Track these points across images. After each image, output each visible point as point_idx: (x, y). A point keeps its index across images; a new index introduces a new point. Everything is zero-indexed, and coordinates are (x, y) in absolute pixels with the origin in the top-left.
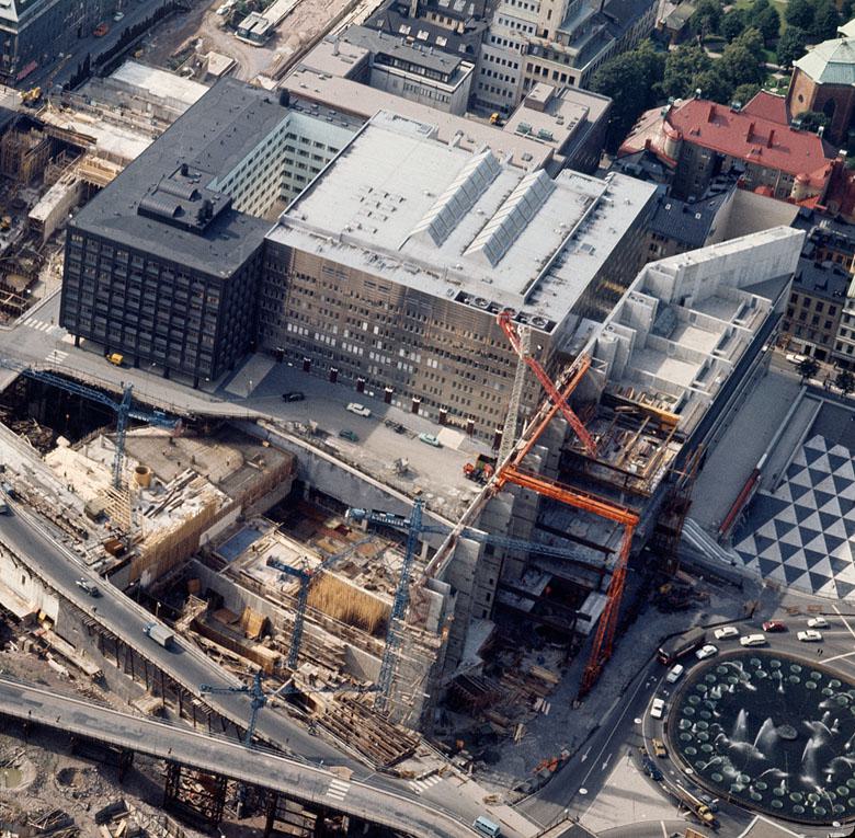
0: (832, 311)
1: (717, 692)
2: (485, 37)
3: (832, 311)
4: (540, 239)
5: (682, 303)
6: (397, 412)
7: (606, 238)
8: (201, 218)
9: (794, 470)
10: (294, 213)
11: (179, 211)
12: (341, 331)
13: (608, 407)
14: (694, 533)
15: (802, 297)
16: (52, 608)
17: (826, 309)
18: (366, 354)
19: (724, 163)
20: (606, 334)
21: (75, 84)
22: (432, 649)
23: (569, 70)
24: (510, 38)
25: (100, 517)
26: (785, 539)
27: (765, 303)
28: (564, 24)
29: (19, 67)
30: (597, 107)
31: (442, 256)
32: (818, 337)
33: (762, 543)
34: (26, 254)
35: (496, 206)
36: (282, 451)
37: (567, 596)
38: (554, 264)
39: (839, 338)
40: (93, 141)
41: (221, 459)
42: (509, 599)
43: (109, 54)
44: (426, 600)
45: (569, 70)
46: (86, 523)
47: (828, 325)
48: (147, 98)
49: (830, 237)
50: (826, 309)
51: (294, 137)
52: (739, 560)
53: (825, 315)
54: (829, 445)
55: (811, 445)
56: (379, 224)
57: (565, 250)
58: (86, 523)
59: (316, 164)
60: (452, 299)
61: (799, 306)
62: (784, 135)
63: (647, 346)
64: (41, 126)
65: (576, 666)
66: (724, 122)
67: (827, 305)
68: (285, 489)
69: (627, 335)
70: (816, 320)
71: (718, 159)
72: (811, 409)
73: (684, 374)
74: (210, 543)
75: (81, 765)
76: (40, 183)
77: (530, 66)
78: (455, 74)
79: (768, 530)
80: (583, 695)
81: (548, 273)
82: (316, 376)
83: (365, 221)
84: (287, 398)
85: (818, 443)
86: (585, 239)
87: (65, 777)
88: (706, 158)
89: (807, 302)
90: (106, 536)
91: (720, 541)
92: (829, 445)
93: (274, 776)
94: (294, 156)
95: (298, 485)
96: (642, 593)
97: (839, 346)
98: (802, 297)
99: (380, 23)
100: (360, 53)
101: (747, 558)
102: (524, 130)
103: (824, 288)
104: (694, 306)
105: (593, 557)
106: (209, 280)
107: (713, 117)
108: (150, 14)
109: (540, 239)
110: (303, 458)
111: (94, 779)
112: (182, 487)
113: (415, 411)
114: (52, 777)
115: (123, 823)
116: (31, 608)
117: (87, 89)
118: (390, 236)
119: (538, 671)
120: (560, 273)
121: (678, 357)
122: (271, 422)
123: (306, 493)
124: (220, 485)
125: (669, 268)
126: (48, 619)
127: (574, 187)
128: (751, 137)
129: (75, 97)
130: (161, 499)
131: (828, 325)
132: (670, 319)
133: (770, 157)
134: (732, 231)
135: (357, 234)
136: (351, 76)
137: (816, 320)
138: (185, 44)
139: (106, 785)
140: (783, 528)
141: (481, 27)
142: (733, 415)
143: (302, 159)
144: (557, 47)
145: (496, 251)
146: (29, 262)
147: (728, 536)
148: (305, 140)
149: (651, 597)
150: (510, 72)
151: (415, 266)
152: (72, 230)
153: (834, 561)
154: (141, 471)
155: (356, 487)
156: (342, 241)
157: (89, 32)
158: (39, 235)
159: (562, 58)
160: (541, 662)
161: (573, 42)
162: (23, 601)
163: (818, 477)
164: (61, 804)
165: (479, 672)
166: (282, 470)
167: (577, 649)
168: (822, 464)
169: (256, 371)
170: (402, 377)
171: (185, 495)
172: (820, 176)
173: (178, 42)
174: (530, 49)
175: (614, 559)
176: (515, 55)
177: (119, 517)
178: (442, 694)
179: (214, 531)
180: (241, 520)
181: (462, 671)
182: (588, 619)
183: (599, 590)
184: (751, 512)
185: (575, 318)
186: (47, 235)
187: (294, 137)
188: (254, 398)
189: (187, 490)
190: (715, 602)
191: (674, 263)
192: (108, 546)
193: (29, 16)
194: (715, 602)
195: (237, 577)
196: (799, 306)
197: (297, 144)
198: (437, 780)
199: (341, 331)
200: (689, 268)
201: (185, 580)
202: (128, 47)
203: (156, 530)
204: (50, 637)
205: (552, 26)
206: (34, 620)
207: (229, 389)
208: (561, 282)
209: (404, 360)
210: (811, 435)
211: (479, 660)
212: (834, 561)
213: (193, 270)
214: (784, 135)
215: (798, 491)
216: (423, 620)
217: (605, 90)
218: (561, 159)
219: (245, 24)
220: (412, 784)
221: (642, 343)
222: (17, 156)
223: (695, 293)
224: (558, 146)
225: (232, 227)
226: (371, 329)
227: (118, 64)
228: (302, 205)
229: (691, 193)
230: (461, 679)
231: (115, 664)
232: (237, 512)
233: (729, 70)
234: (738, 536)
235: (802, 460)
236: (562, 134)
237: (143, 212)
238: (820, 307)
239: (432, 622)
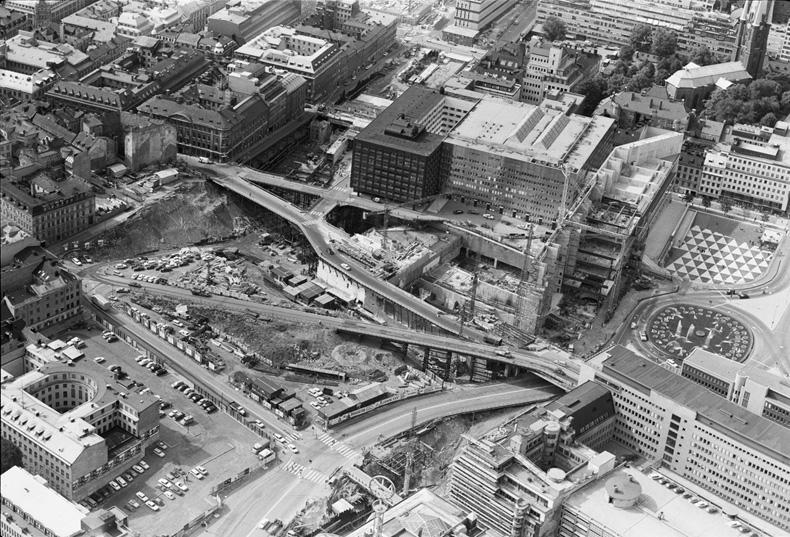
0: (697, 173)
1: (666, 319)
2: (524, 74)
3: (697, 173)
4: (566, 139)
5: (632, 164)
6: (506, 217)
8: (413, 133)
9: (687, 239)
10: (453, 132)
11: (403, 131)
12: (478, 182)
13: (606, 202)
14: (647, 260)
15: (683, 167)
16: (361, 296)
17: (695, 171)
18: (490, 191)
20: (602, 172)
21: (339, 103)
22: (541, 292)
23: (564, 87)
24: (535, 74)
25: (379, 258)
27: (669, 164)
28: (560, 67)
29: (315, 95)
30: (580, 99)
31: (524, 146)
32: (692, 186)
34: (326, 169)
36: (456, 235)
37: (594, 283)
38: (573, 148)
39: (702, 185)
40: (351, 123)
41: (428, 239)
42: (570, 282)
43: (353, 91)
44: (537, 270)
45: (564, 87)
46: (374, 260)
47: (696, 179)
48: (373, 107)
49: (692, 144)
50: (695, 171)
53: (694, 175)
54: (702, 230)
55: (694, 229)
57: (577, 143)
58: (374, 260)
59: (451, 124)
61: (682, 172)
62: (666, 104)
63: (619, 181)
64: (327, 119)
65: (601, 311)
66: (638, 100)
67: (695, 170)
68: (457, 252)
69: (611, 173)
70: (690, 177)
71: (638, 115)
72: (692, 215)
73: (639, 189)
74: (427, 272)
75: (386, 353)
76: (328, 142)
78: (513, 89)
79: (679, 261)
80: (607, 322)
81: (571, 151)
82: (473, 204)
83: (486, 134)
84: (456, 213)
85: (697, 228)
87: (379, 357)
88: (632, 117)
89: (686, 170)
90: (383, 265)
91: (659, 264)
92: (702, 230)
93: (473, 350)
94: (447, 123)
95: (463, 250)
96: (627, 283)
97: (702, 188)
98: (683, 167)
100: (469, 81)
103: (693, 162)
105: (607, 263)
106: (419, 157)
107: (633, 98)
108: (369, 76)
109: (566, 139)
110: (466, 237)
111: (391, 358)
112: (412, 249)
113: (514, 216)
114: (373, 357)
115: (408, 373)
116: (352, 298)
117: (345, 104)
118: (498, 139)
119: (585, 313)
121: (633, 185)
122: (449, 222)
123: (467, 254)
124: (430, 248)
125: (625, 149)
126: (360, 302)
127: (577, 122)
128: (651, 106)
129: (340, 107)
130: (404, 253)
131: (696, 179)
132: (627, 170)
133: (660, 114)
134: (648, 135)
136: (466, 88)
137: (690, 177)
138: (385, 89)
139: (397, 361)
140: (686, 261)
141: (521, 71)
142: (659, 214)
143: (451, 118)
144: (558, 77)
145: (548, 142)
146: (328, 172)
147: (663, 262)
148: (453, 109)
149: (632, 284)
150: (537, 89)
151: (511, 150)
153: (711, 273)
154: (394, 242)
155: (491, 247)
156: (476, 142)
157: (343, 82)
158: (331, 161)
160: (586, 310)
161: (564, 75)
162: (348, 295)
164: (379, 367)
165: (558, 313)
166: (457, 242)
167: (601, 305)
168: (700, 236)
169: (440, 203)
170: (507, 200)
171: (413, 252)
172: (685, 120)
173: (381, 88)
174: (545, 78)
175: (615, 263)
176: (537, 82)
177: (389, 258)
178: (543, 322)
179: (428, 266)
180: (440, 263)
181: (551, 312)
182: (607, 287)
183: (609, 279)
184: (670, 255)
185: (585, 172)
186: (335, 161)
188: (442, 212)
189: (415, 250)
190: (660, 286)
191: (627, 146)
192: (384, 268)
193: (319, 72)
194: (660, 286)
195: (443, 285)
196: (682, 172)
197: (449, 111)
198: (547, 351)
199: (478, 182)
201: (417, 282)
202: (361, 87)
203: (403, 265)
204: (361, 310)
205: (555, 68)
206: (353, 303)
207: (429, 210)
208: (577, 155)
209: (508, 193)
210: (693, 226)
211: (558, 308)
212: (711, 273)
213: (412, 154)
214: (666, 104)
215: (690, 247)
216: (536, 280)
217: (582, 93)
219: (412, 79)
220: (535, 353)
222: (317, 131)
223: (637, 161)
225: (427, 138)
226: (492, 180)
227: (358, 95)
228: (457, 129)
229: (628, 126)
230: (551, 315)
231: (392, 317)
232: (438, 259)
233: (637, 84)
234: (667, 264)
237: (387, 133)
238: (692, 171)
239: (540, 281)
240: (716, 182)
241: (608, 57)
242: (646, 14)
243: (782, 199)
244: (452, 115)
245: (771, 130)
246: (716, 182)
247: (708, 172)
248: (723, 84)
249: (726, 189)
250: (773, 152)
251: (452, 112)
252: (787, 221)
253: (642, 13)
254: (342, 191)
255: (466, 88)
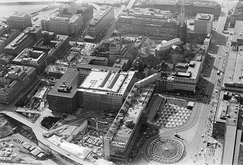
7: (128, 81)
19: (223, 46)
26: (165, 114)
33: (160, 121)
35: (111, 78)
51: (81, 75)
52: (157, 124)
55: (165, 105)
56: (94, 85)
60: (106, 94)
77: (116, 57)
79: (160, 119)
81: (120, 87)
86: (125, 81)
99: (93, 55)
101: (158, 124)
102: (116, 66)
104: (143, 88)
109: (119, 83)
120: (122, 87)
135: (91, 87)
136: (89, 64)
145: (111, 87)
152: (48, 95)
159: (121, 54)
163: (167, 109)
184: (156, 117)
187: (81, 75)
197: (81, 76)
200: (141, 83)
218: (122, 70)
221: (136, 95)
224: (121, 68)
235: (164, 107)
236: (122, 66)
240: (172, 86)
241: (139, 39)
242: (149, 23)
243: (193, 90)
244: (83, 77)
245: (188, 65)
246: (172, 86)
247: (168, 84)
248: (174, 47)
249: (175, 88)
250: (188, 75)
251: (83, 76)
252: (242, 22)
253: (148, 22)
254: (46, 112)
255: (89, 64)
